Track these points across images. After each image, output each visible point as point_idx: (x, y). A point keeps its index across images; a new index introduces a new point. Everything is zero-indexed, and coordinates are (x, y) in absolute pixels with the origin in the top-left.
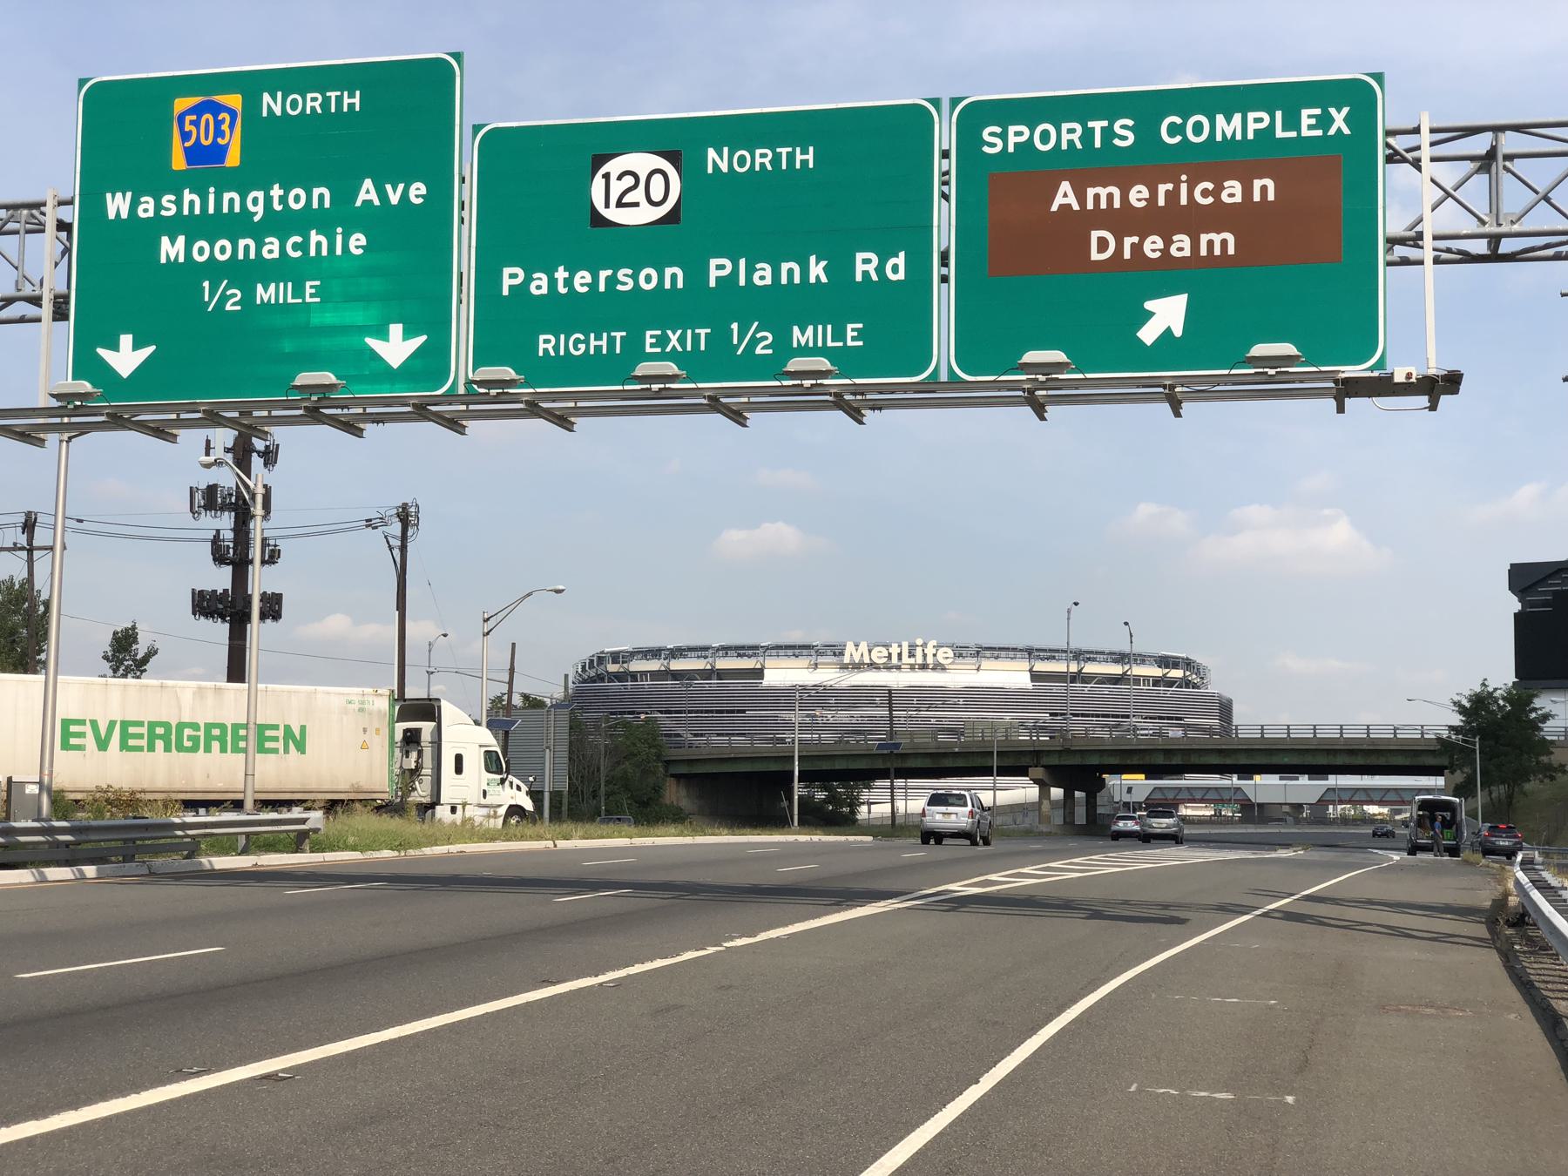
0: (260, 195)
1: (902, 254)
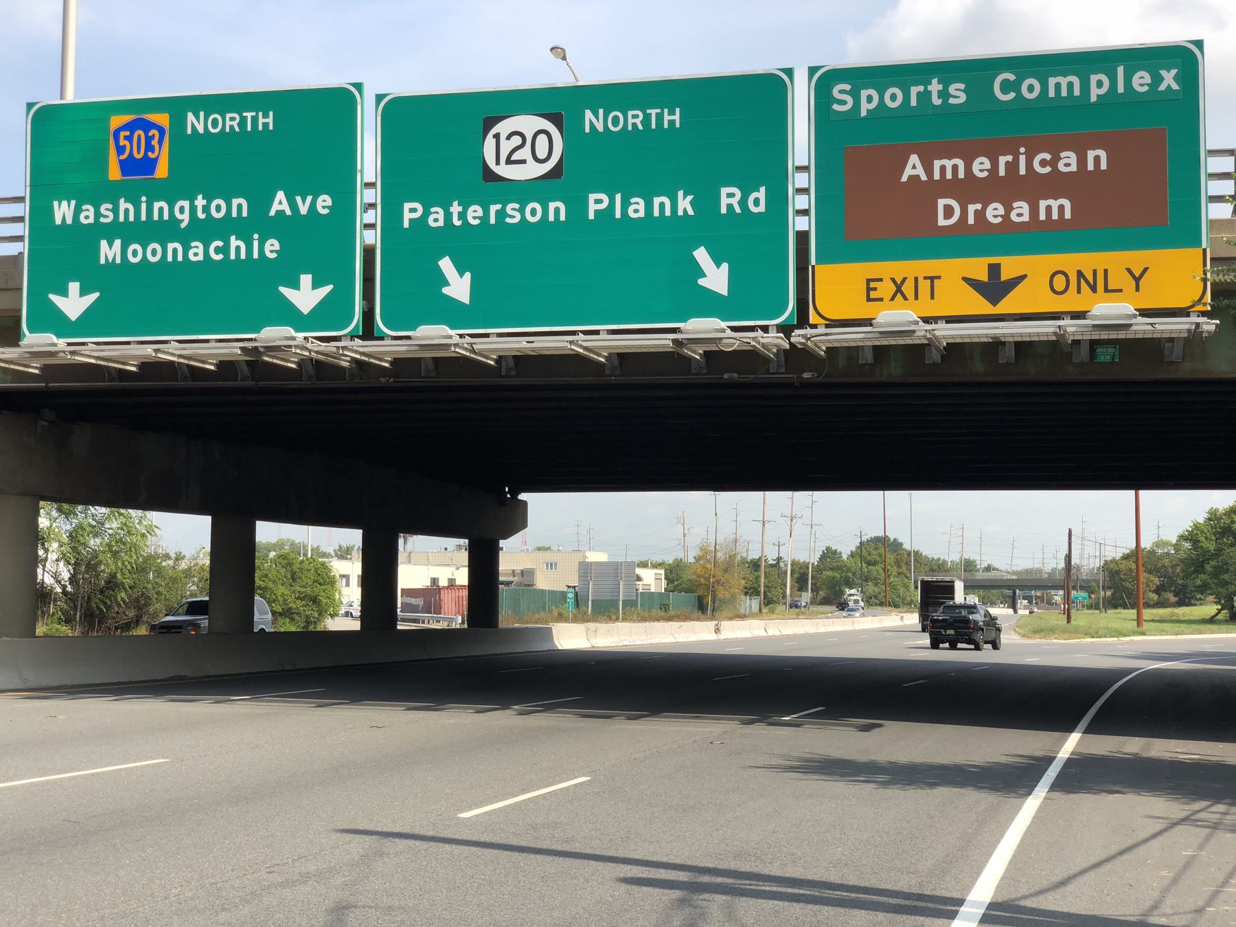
0: (186, 204)
1: (763, 189)
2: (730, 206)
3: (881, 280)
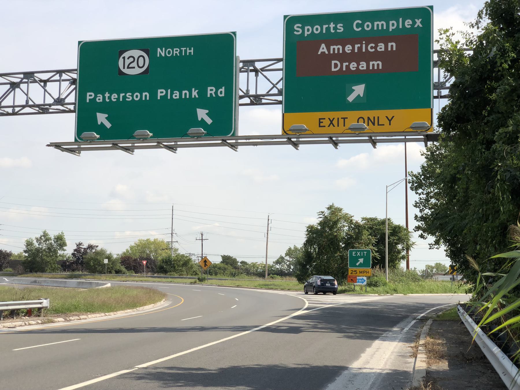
1: (223, 88)
2: (211, 94)
3: (325, 119)
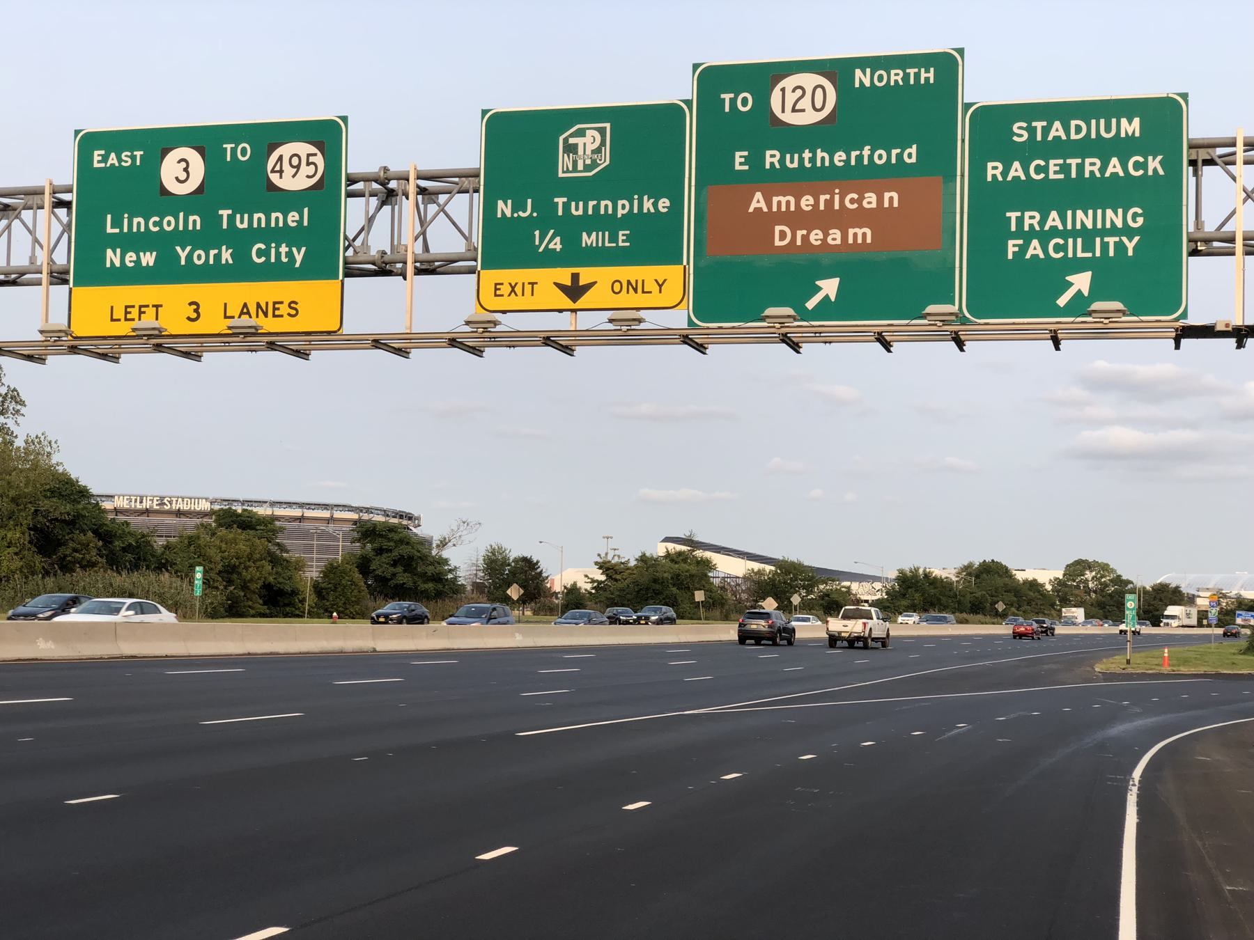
1: (914, 147)
